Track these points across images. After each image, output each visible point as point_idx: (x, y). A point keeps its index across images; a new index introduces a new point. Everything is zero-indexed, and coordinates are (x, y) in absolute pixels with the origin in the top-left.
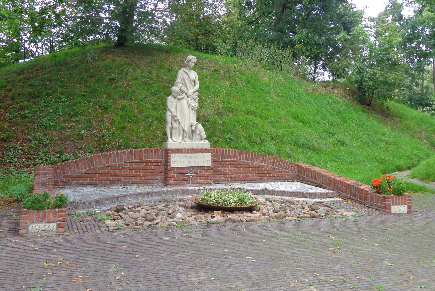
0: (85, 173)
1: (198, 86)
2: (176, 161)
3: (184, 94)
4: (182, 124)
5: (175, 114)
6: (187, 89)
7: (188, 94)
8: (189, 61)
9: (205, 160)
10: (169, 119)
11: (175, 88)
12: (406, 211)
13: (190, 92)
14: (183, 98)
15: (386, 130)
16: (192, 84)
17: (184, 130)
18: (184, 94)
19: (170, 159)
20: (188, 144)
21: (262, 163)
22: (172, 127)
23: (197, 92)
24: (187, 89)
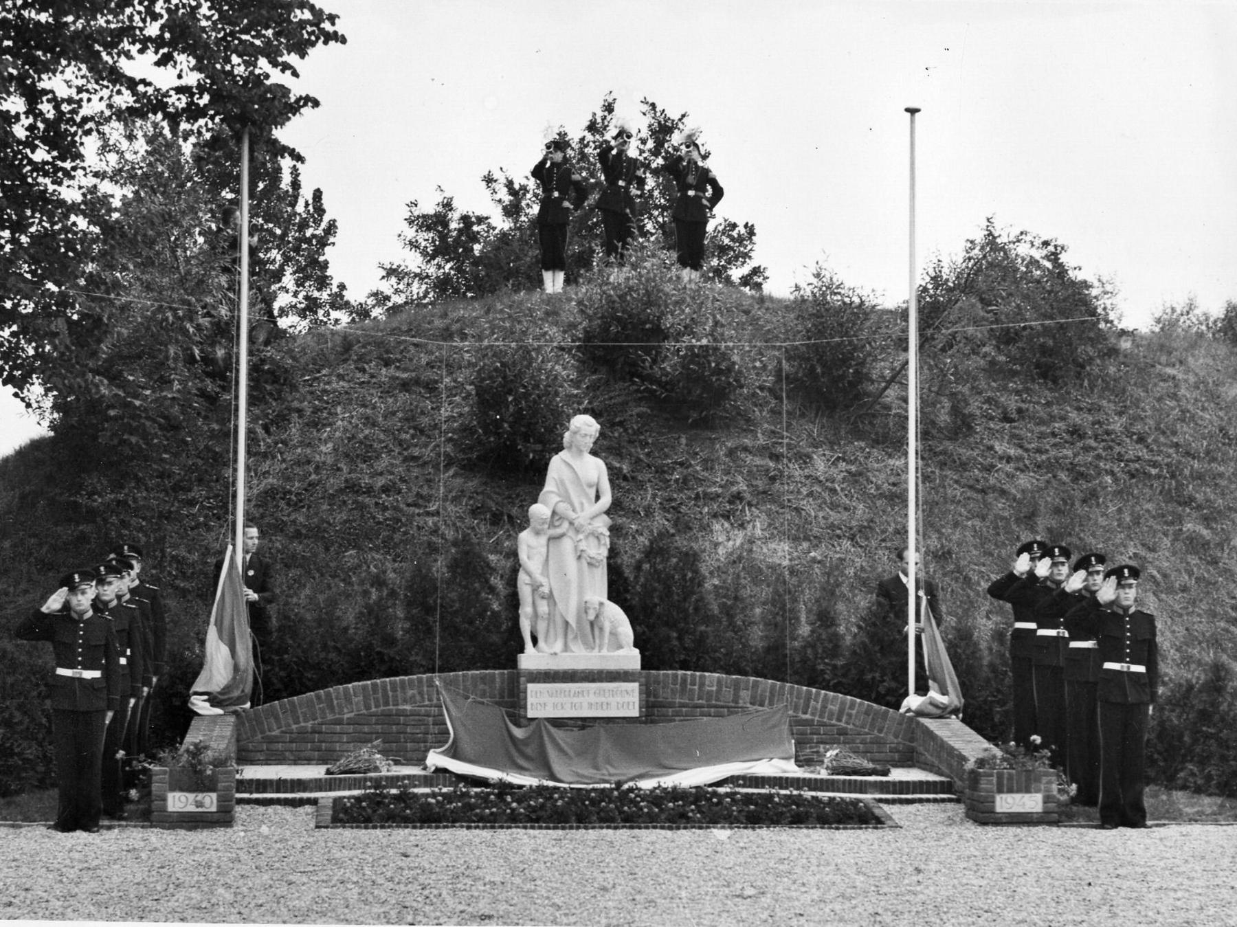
0: (314, 732)
2: (542, 702)
3: (566, 525)
4: (560, 606)
5: (541, 579)
7: (576, 523)
9: (625, 701)
11: (539, 510)
12: (634, 712)
14: (563, 535)
15: (887, 834)
16: (587, 495)
17: (567, 623)
18: (566, 525)
19: (526, 698)
20: (580, 658)
21: (805, 713)
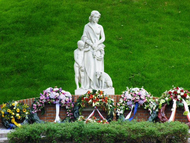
1: (103, 39)
3: (90, 47)
4: (88, 74)
6: (92, 42)
7: (93, 46)
8: (92, 16)
10: (76, 69)
13: (95, 45)
14: (89, 50)
17: (90, 80)
18: (90, 47)
22: (80, 78)
23: (103, 44)
24: (92, 42)
